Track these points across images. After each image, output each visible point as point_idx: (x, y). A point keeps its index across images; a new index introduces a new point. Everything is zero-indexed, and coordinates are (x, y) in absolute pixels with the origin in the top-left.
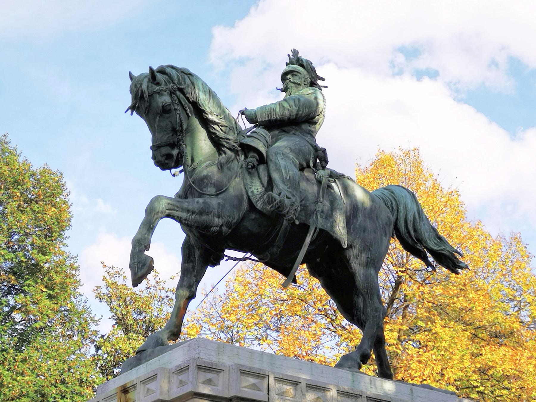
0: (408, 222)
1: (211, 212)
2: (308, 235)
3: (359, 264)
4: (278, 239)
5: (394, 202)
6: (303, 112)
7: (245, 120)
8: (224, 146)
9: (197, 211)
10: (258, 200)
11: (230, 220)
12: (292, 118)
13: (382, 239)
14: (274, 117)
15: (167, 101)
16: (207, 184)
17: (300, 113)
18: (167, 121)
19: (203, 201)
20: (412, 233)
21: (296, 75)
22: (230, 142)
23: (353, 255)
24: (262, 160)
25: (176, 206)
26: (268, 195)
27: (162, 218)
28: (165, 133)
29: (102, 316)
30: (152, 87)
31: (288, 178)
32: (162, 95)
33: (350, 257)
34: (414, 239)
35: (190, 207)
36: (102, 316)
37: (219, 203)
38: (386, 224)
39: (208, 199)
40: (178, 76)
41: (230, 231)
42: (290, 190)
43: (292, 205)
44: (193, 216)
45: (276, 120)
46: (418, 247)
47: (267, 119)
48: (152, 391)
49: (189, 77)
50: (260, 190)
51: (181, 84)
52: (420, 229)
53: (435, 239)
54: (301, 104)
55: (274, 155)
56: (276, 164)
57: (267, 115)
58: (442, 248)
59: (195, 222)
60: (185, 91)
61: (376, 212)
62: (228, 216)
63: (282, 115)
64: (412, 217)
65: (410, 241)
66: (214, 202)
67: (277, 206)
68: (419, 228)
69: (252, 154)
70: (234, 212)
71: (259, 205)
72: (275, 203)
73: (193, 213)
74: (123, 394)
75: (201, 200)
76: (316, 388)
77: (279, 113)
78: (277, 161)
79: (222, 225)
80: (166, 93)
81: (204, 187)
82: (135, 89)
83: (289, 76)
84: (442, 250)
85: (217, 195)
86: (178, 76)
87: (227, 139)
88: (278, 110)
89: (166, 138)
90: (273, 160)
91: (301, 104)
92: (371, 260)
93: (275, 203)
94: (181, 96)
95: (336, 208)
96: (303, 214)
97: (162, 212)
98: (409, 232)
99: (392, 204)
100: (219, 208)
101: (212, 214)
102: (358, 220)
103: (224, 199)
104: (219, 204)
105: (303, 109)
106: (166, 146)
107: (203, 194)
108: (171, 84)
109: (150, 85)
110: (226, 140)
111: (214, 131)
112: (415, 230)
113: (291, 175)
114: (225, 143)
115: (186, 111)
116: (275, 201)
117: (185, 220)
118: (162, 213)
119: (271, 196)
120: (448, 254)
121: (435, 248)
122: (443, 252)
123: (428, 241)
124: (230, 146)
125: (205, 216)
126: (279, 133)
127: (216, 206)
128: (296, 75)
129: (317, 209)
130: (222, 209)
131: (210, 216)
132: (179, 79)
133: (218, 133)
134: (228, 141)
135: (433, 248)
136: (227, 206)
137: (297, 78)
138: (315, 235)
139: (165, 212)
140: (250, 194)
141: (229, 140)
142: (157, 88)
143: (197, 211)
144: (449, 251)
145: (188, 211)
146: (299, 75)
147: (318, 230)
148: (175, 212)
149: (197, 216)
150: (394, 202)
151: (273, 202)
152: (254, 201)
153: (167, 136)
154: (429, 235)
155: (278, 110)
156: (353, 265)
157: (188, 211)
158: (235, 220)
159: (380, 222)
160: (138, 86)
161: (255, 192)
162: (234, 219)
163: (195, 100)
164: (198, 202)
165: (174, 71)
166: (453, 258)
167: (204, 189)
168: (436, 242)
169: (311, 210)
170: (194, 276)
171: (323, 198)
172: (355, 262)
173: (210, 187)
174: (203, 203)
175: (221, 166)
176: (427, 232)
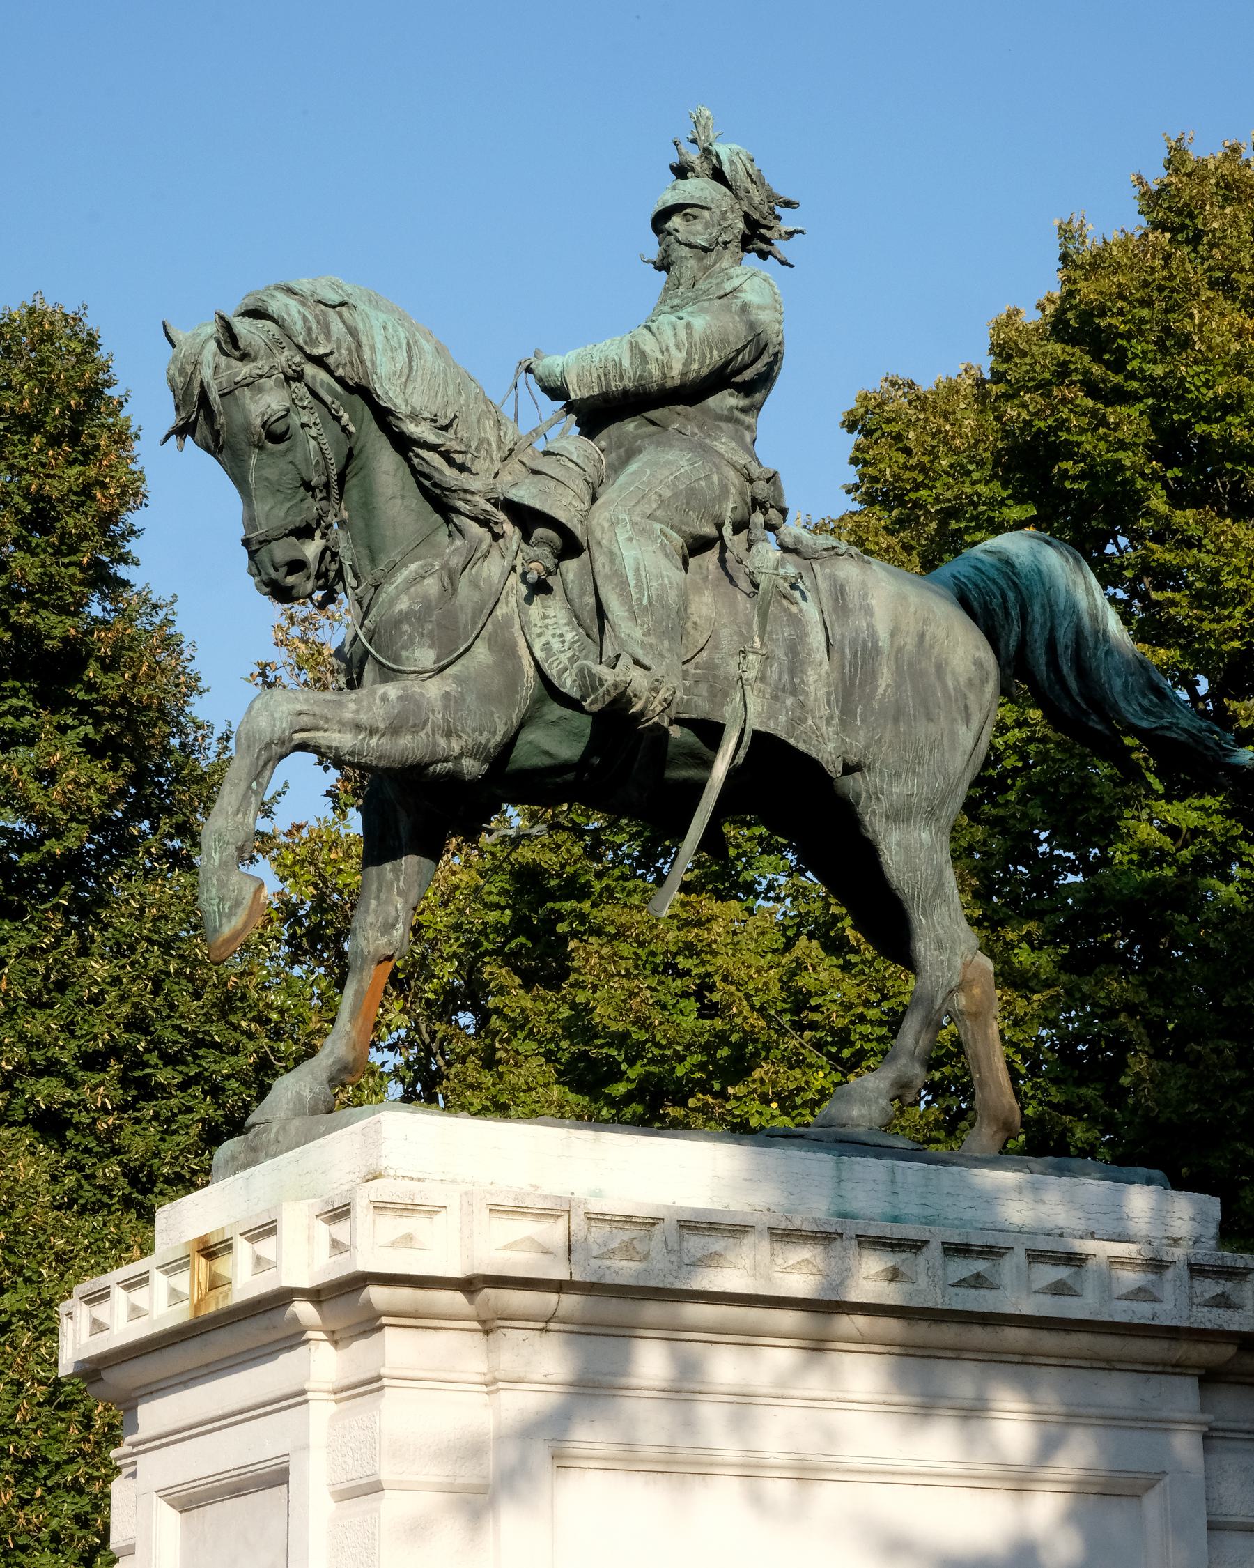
0: (1060, 649)
1: (426, 722)
2: (721, 754)
3: (887, 817)
4: (636, 766)
5: (1011, 596)
6: (702, 363)
7: (536, 389)
8: (458, 512)
9: (382, 726)
10: (565, 670)
11: (482, 739)
12: (669, 384)
13: (953, 734)
14: (616, 385)
15: (275, 406)
16: (411, 638)
17: (695, 366)
18: (283, 464)
19: (400, 693)
20: (1073, 684)
21: (695, 217)
22: (477, 499)
23: (867, 792)
24: (570, 546)
25: (322, 717)
26: (581, 670)
27: (281, 757)
28: (281, 497)
29: (286, 785)
30: (228, 367)
31: (645, 601)
32: (260, 390)
33: (858, 795)
34: (1078, 699)
35: (363, 718)
36: (286, 785)
37: (447, 693)
38: (970, 683)
39: (414, 685)
40: (305, 319)
41: (486, 767)
42: (652, 640)
43: (656, 690)
44: (374, 741)
45: (625, 392)
46: (1091, 724)
47: (596, 391)
48: (268, 1261)
49: (340, 315)
50: (569, 637)
51: (314, 343)
52: (1098, 667)
53: (1144, 696)
54: (696, 337)
55: (606, 525)
56: (612, 556)
57: (595, 375)
58: (1164, 722)
59: (380, 757)
60: (331, 361)
61: (936, 651)
62: (474, 730)
63: (641, 377)
64: (1071, 635)
65: (1066, 707)
66: (433, 689)
67: (608, 699)
68: (1094, 665)
69: (540, 532)
70: (492, 714)
71: (569, 682)
72: (601, 690)
73: (372, 732)
74: (203, 1260)
75: (392, 690)
76: (709, 1229)
77: (630, 373)
78: (616, 550)
79: (461, 755)
80: (270, 383)
81: (404, 647)
82: (180, 381)
83: (676, 221)
84: (1168, 728)
85: (442, 669)
86: (305, 319)
87: (466, 491)
88: (626, 363)
89: (282, 514)
90: (604, 542)
91: (696, 337)
92: (920, 801)
93: (601, 690)
94: (323, 375)
95: (802, 663)
96: (705, 693)
97: (282, 742)
98: (1061, 680)
99: (1005, 600)
100: (446, 707)
101: (428, 729)
102: (877, 686)
103: (458, 679)
104: (447, 695)
105: (703, 354)
106: (287, 535)
107: (402, 672)
108: (286, 353)
109: (223, 360)
110: (462, 495)
111: (427, 470)
112: (1082, 671)
113: (653, 592)
114: (459, 504)
115: (338, 419)
116: (602, 685)
117: (352, 753)
118: (283, 743)
119: (589, 671)
120: (1183, 737)
121: (1144, 724)
122: (1168, 734)
123: (1122, 704)
124: (477, 511)
125: (409, 737)
126: (636, 428)
127: (438, 705)
128: (695, 217)
129: (745, 676)
130: (456, 711)
131: (422, 734)
132: (309, 329)
133: (436, 476)
134: (469, 497)
135: (1138, 722)
136: (471, 699)
137: (698, 226)
138: (742, 753)
139: (291, 739)
140: (539, 655)
141: (473, 493)
142: (244, 370)
143: (382, 726)
144: (1184, 730)
145: (358, 727)
146: (706, 214)
147: (747, 740)
148: (320, 734)
149: (383, 740)
150: (1011, 596)
151: (595, 689)
152: (552, 673)
153: (287, 505)
154: (1126, 683)
155: (626, 363)
156: (867, 818)
157: (358, 727)
158: (498, 738)
159: (950, 683)
160: (189, 369)
161: (556, 644)
162: (494, 734)
163: (364, 382)
164: (384, 698)
165: (293, 304)
166: (1200, 748)
167: (404, 653)
168: (1145, 702)
169: (726, 678)
170: (399, 894)
171: (762, 639)
172: (874, 813)
173: (421, 645)
174: (400, 698)
175: (450, 578)
176: (1119, 676)
